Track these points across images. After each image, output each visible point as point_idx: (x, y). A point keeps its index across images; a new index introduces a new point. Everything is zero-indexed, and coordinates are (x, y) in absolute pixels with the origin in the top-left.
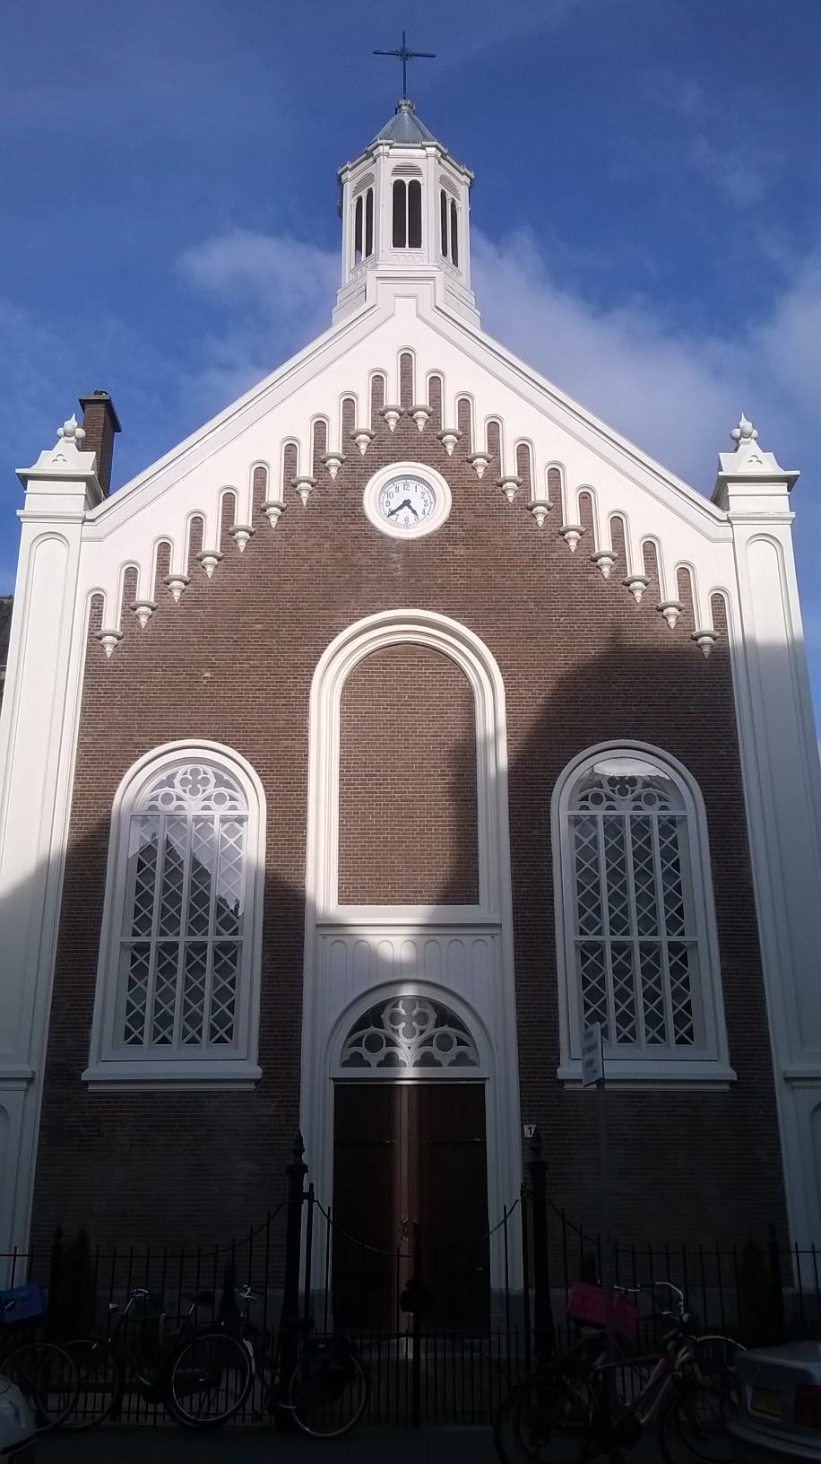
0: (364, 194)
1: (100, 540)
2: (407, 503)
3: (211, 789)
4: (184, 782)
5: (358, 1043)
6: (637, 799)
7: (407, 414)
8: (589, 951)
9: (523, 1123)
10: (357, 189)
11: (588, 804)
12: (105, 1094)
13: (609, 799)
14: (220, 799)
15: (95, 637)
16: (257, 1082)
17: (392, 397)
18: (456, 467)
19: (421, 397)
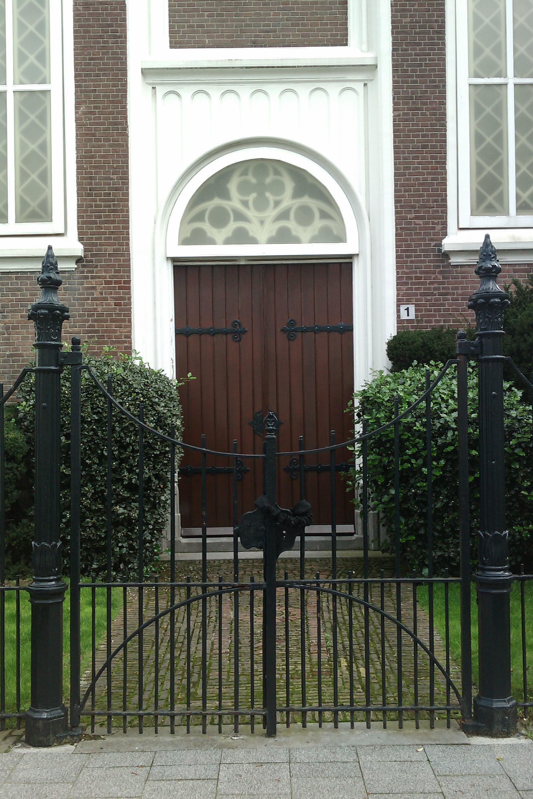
5: (199, 217)
16: (79, 260)
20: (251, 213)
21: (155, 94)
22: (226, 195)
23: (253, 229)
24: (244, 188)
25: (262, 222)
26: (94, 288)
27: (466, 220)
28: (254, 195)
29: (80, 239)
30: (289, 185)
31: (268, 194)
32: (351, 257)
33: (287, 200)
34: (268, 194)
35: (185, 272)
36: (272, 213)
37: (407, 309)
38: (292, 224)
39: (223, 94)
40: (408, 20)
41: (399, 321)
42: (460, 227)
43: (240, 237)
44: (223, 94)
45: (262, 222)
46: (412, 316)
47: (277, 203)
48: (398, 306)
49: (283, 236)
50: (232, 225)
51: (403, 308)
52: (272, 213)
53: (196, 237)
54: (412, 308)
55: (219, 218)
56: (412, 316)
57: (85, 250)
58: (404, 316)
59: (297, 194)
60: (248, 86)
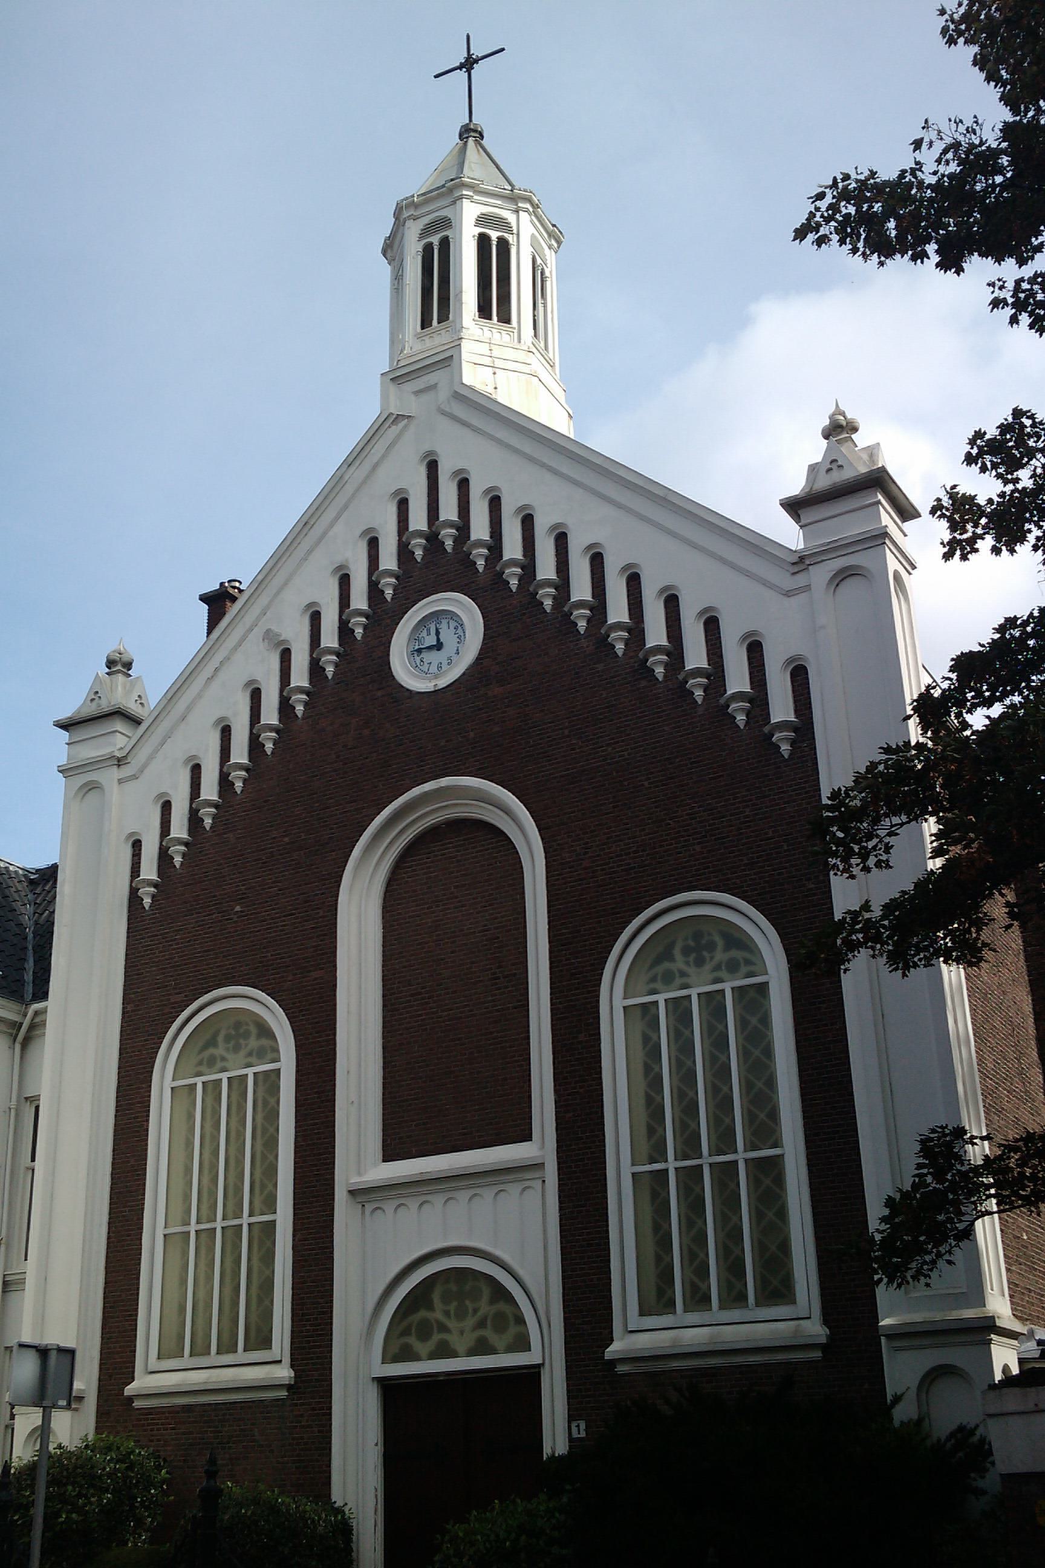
0: (435, 240)
1: (134, 777)
2: (439, 646)
3: (720, 956)
4: (686, 951)
5: (406, 1332)
6: (718, 968)
7: (432, 538)
8: (270, 1204)
9: (571, 1418)
10: (426, 231)
11: (723, 974)
12: (149, 1411)
13: (683, 974)
14: (733, 967)
15: (134, 893)
16: (289, 1387)
17: (418, 521)
18: (488, 590)
19: (449, 511)
20: (452, 1324)
21: (363, 1213)
22: (430, 1307)
23: (456, 1341)
24: (446, 1299)
25: (462, 1333)
26: (302, 1416)
27: (153, 1363)
28: (455, 1303)
29: (292, 1366)
30: (486, 1292)
31: (467, 1302)
32: (539, 1366)
33: (485, 1307)
34: (467, 1302)
35: (391, 1391)
36: (470, 1322)
37: (578, 1426)
38: (488, 1333)
39: (524, 1189)
40: (571, 1115)
41: (571, 1440)
42: (150, 1370)
43: (444, 1351)
44: (396, 1209)
45: (462, 1333)
46: (583, 1434)
47: (475, 1311)
48: (569, 1423)
49: (482, 1348)
50: (436, 1337)
51: (574, 1425)
52: (470, 1322)
53: (406, 1354)
54: (583, 1425)
55: (424, 1331)
56: (583, 1434)
57: (296, 1377)
58: (575, 1435)
59: (492, 1301)
60: (515, 1184)
